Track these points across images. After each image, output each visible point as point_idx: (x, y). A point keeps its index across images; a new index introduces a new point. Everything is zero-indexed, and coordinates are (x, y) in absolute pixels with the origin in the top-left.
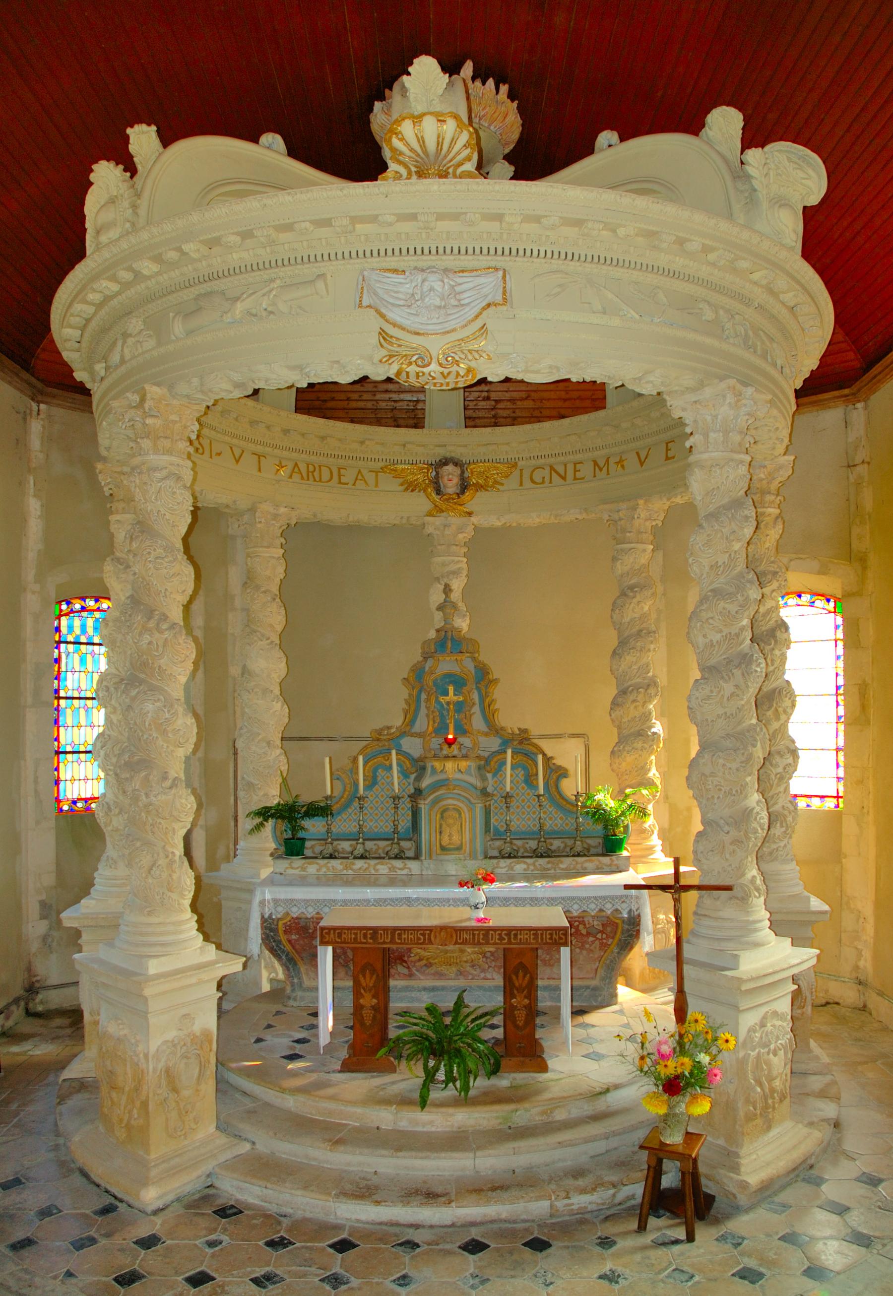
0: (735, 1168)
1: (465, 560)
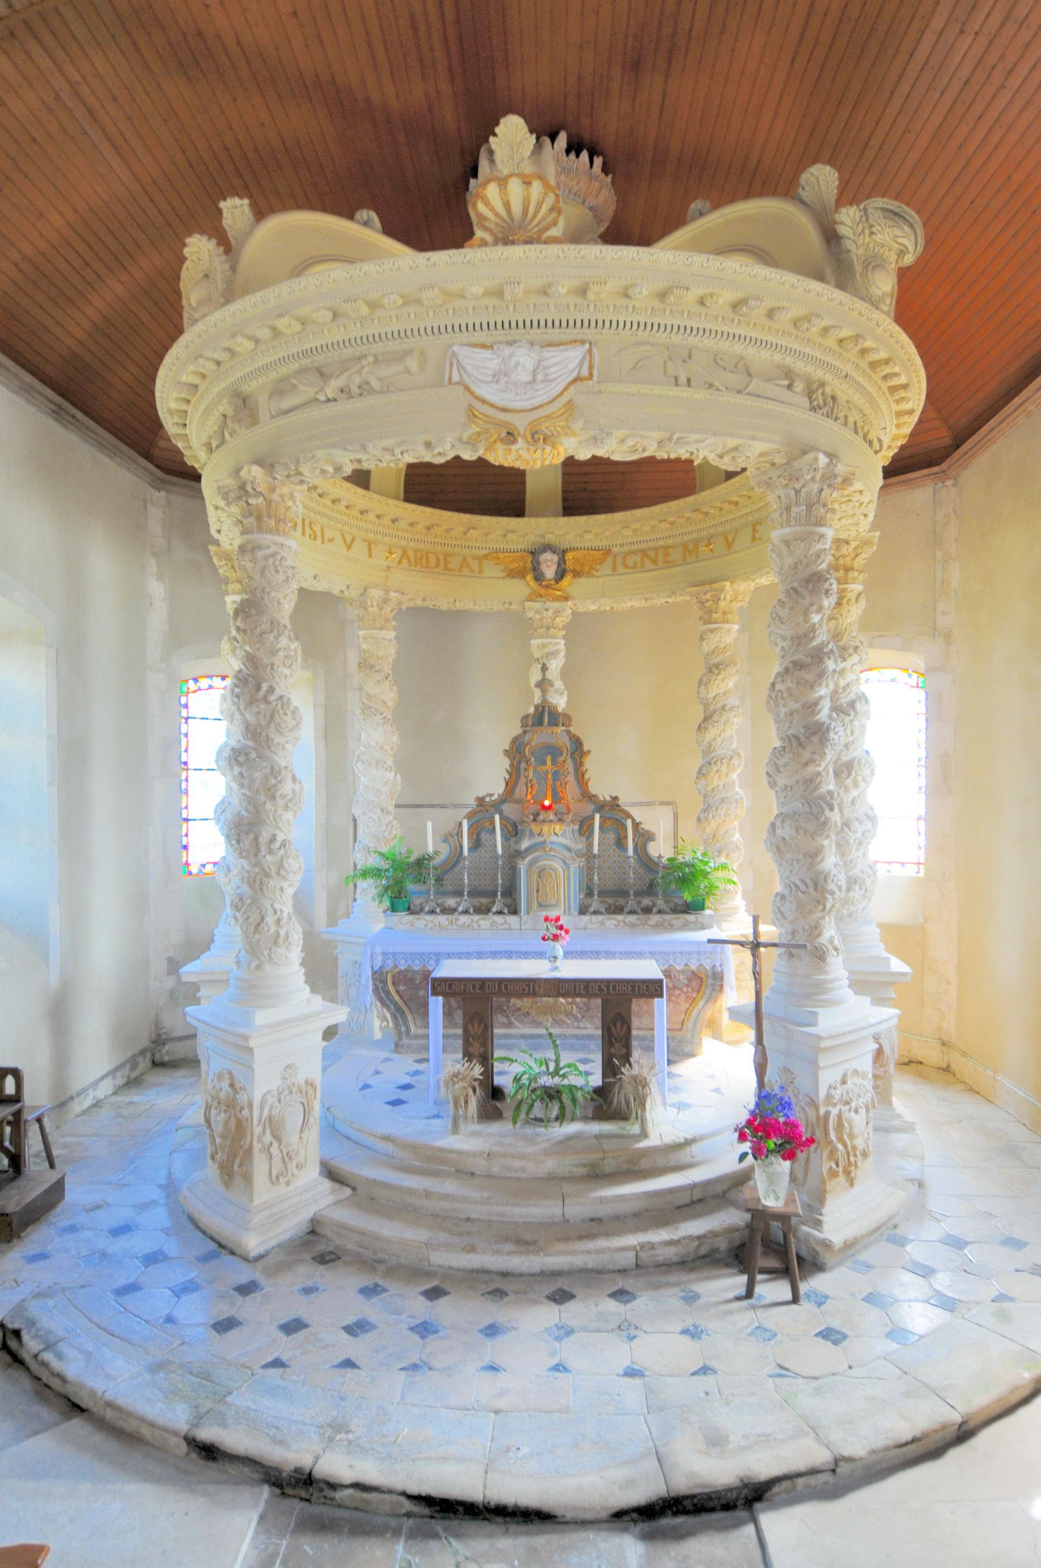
0: (818, 1224)
1: (563, 642)
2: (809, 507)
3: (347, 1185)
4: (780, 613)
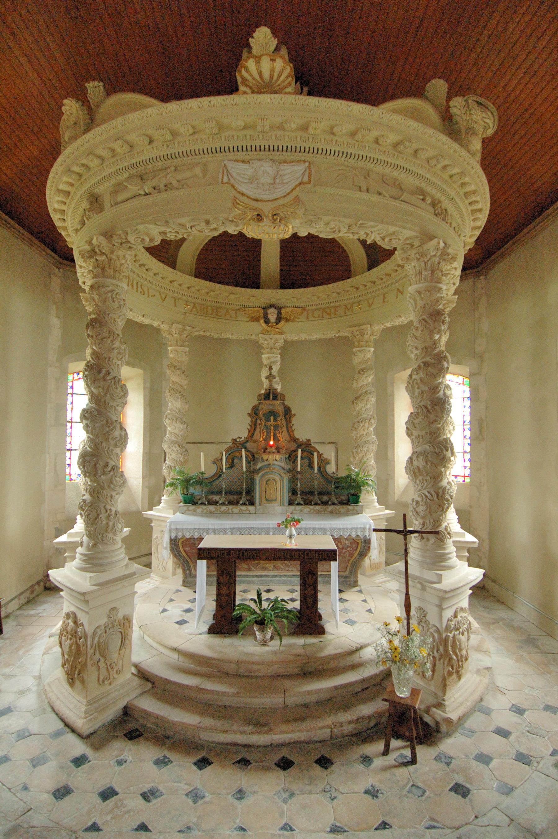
2: (433, 272)
3: (149, 681)
4: (415, 334)
